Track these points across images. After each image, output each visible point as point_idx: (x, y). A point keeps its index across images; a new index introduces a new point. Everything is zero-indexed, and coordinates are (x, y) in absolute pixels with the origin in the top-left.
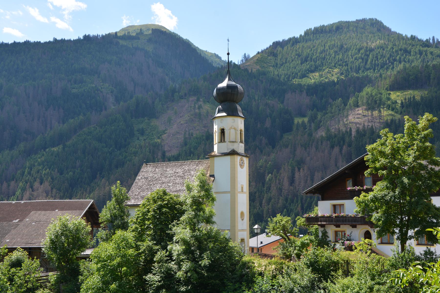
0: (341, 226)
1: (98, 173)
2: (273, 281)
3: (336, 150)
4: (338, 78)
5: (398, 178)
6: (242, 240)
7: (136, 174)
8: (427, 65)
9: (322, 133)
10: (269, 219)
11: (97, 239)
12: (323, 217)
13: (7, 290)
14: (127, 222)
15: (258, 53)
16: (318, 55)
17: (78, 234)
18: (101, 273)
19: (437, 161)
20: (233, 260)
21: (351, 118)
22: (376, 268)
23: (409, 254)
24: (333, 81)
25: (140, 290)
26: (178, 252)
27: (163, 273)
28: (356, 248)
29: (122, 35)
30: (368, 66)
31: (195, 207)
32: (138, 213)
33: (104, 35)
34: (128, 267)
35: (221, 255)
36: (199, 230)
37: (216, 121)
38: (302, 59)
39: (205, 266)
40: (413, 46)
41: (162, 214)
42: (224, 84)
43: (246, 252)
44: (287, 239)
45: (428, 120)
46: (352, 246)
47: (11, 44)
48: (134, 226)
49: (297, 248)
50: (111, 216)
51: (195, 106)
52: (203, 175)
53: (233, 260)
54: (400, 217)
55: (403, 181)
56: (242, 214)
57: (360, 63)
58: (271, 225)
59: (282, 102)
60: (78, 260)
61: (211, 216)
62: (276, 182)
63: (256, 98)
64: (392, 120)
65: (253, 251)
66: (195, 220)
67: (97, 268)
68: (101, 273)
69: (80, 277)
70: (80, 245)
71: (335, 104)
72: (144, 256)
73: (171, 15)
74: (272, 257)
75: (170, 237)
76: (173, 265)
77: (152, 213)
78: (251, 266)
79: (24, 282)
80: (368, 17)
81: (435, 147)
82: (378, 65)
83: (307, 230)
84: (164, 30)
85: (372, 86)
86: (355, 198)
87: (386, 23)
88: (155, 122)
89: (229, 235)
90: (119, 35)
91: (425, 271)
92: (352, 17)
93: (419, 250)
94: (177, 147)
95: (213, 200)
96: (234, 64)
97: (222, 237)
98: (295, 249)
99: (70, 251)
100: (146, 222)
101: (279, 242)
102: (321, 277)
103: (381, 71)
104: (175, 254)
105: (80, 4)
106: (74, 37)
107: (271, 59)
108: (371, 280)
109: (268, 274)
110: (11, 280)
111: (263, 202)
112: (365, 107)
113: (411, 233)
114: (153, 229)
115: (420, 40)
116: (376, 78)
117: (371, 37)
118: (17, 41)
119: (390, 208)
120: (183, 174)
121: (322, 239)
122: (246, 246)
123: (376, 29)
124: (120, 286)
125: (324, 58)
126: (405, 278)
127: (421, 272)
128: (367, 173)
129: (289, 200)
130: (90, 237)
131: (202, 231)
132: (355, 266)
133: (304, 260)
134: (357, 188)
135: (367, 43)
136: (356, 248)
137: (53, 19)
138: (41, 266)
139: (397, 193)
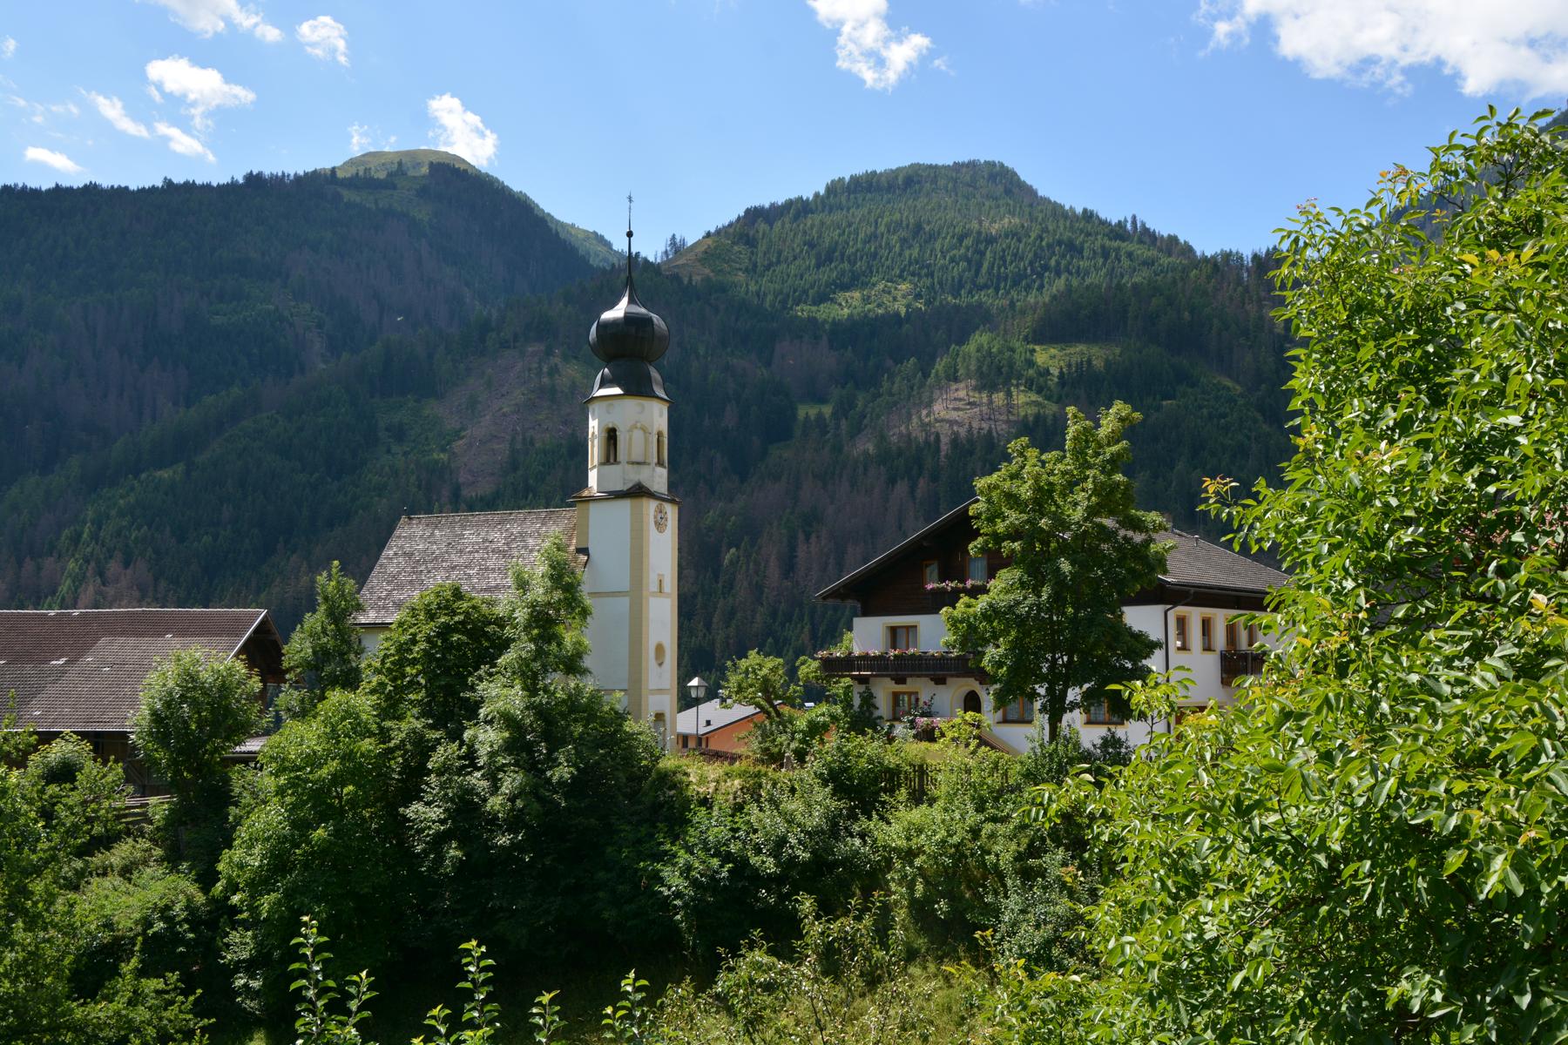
0: (909, 680)
1: (281, 539)
2: (737, 819)
3: (901, 488)
4: (908, 306)
5: (1049, 560)
6: (659, 717)
7: (382, 545)
8: (1118, 284)
9: (866, 445)
10: (729, 663)
11: (277, 712)
12: (865, 657)
13: (38, 840)
14: (357, 671)
15: (708, 235)
16: (859, 245)
17: (226, 698)
18: (288, 800)
19: (1139, 520)
20: (633, 766)
21: (938, 407)
22: (989, 781)
23: (1066, 746)
24: (897, 314)
25: (391, 843)
26: (491, 746)
27: (452, 800)
28: (943, 735)
29: (348, 175)
30: (981, 280)
31: (535, 631)
32: (386, 645)
33: (302, 173)
34: (358, 786)
35: (603, 756)
36: (546, 690)
37: (594, 408)
38: (818, 256)
39: (561, 783)
40: (1089, 234)
41: (449, 647)
42: (617, 312)
43: (668, 746)
44: (773, 714)
45: (1121, 420)
46: (934, 729)
47: (49, 191)
48: (375, 680)
49: (797, 736)
50: (314, 653)
51: (540, 368)
52: (559, 549)
53: (633, 766)
54: (1049, 656)
55: (1058, 568)
56: (660, 649)
57: (964, 271)
58: (734, 679)
59: (768, 364)
60: (226, 767)
61: (578, 655)
62: (748, 570)
63: (702, 351)
64: (1038, 417)
65: (685, 745)
66: (537, 666)
67: (278, 786)
68: (288, 800)
69: (233, 810)
70: (230, 727)
71: (900, 371)
72: (402, 756)
73: (480, 125)
74: (733, 759)
75: (471, 710)
76: (476, 780)
77: (424, 645)
78: (681, 782)
79: (83, 820)
80: (983, 157)
81: (1136, 485)
82: (1006, 279)
83: (824, 689)
84: (463, 167)
85: (991, 331)
86: (945, 609)
87: (1026, 176)
88: (432, 408)
89: (625, 702)
90: (340, 175)
91: (1099, 785)
92: (944, 156)
93: (1091, 737)
94: (493, 474)
95: (585, 613)
96: (646, 260)
97: (606, 708)
98: (793, 739)
99: (206, 742)
100: (408, 669)
101: (752, 721)
102: (856, 807)
103: (1014, 293)
104: (483, 751)
105: (238, 90)
106: (219, 178)
107: (740, 253)
108: (977, 811)
109: (723, 802)
110: (47, 814)
111: (715, 620)
112: (973, 382)
113: (1073, 694)
114: (425, 686)
115: (1104, 223)
116: (1002, 310)
117: (990, 207)
118: (65, 183)
119: (1027, 634)
120: (507, 544)
121: (862, 712)
122: (668, 732)
123: (1001, 189)
124: (337, 833)
125: (875, 256)
126: (1054, 805)
127: (1090, 788)
128: (973, 547)
129: (780, 613)
130: (258, 706)
131: (554, 693)
132: (940, 777)
133: (814, 765)
134: (950, 585)
135: (980, 223)
136: (943, 735)
137: (163, 129)
138: (127, 781)
139: (1045, 597)
